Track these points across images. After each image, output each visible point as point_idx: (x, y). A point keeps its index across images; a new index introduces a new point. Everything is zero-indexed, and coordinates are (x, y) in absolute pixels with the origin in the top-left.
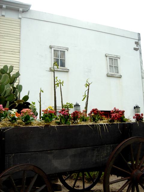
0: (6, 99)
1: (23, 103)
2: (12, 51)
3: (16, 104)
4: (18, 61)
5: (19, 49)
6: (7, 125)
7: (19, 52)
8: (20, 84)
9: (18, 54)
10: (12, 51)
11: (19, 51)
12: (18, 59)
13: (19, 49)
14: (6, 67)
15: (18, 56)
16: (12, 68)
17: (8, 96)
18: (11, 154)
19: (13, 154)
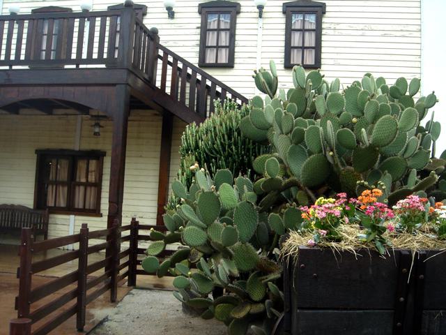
0: (409, 163)
1: (443, 168)
2: (402, 31)
3: (435, 178)
4: (418, 52)
5: (418, 22)
6: (430, 244)
7: (420, 31)
8: (435, 120)
9: (418, 34)
10: (402, 31)
11: (418, 27)
12: (418, 46)
13: (418, 22)
14: (401, 81)
15: (417, 40)
16: (417, 84)
17: (414, 155)
18: (437, 309)
19: (441, 309)
